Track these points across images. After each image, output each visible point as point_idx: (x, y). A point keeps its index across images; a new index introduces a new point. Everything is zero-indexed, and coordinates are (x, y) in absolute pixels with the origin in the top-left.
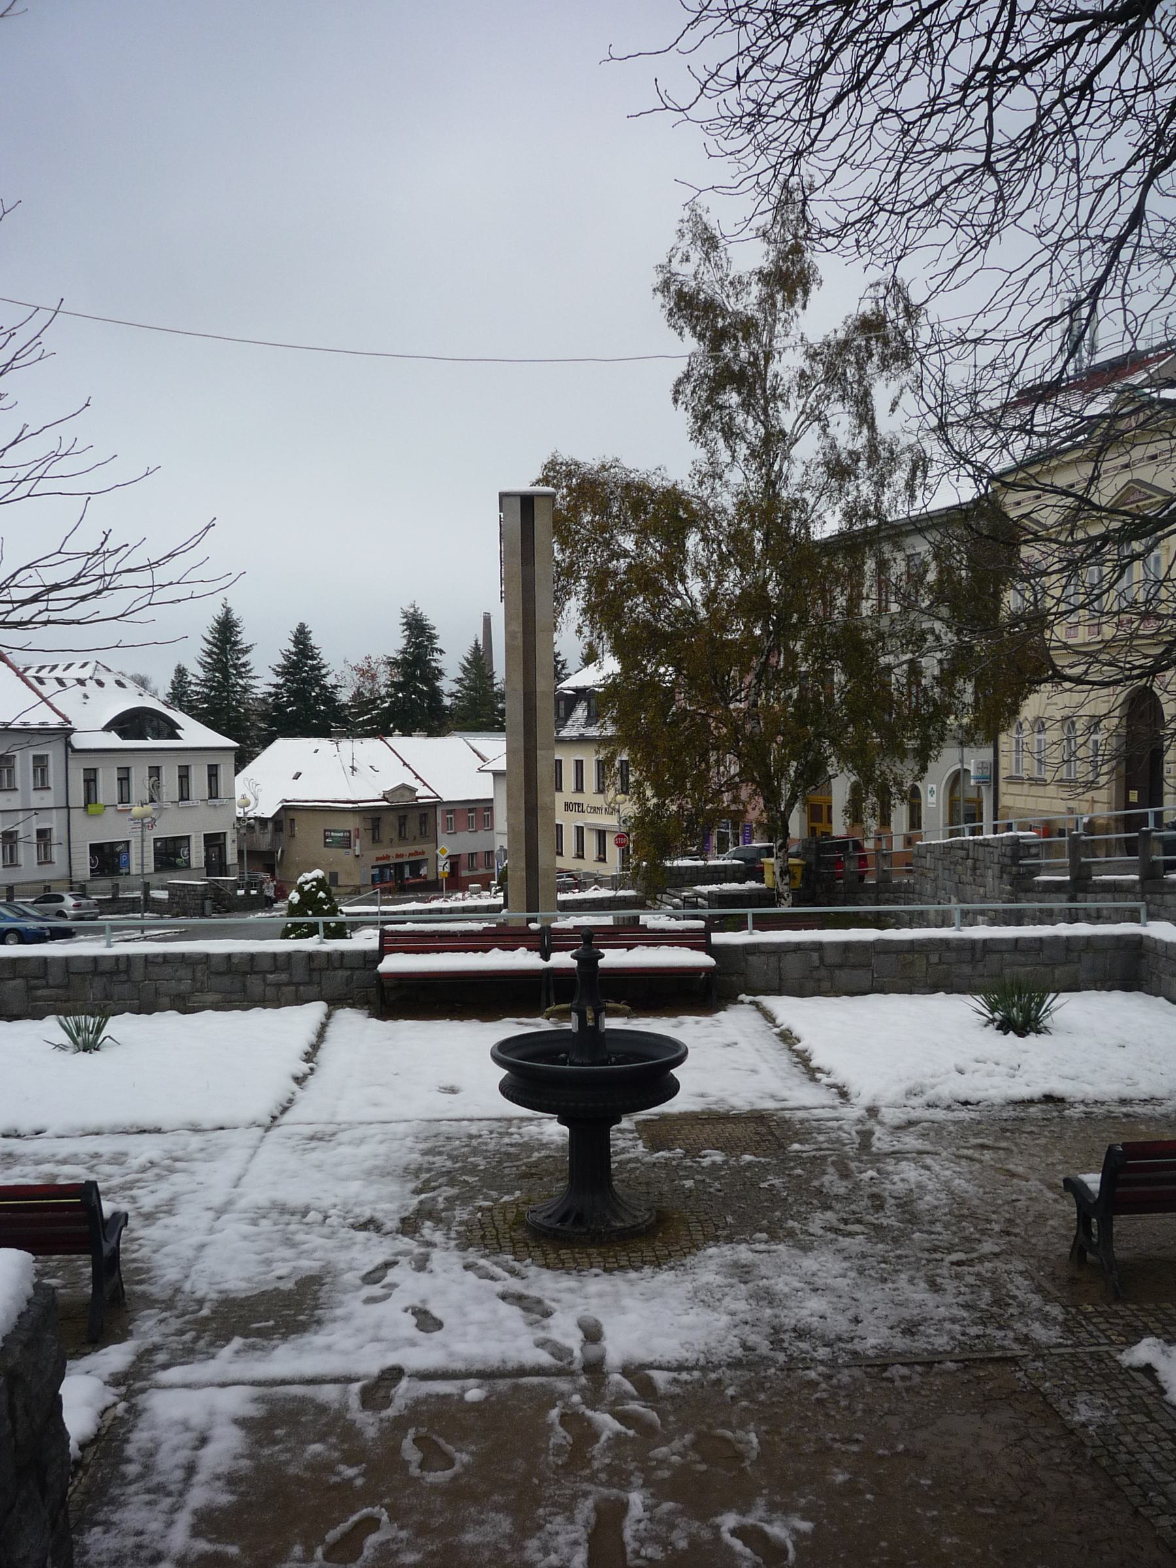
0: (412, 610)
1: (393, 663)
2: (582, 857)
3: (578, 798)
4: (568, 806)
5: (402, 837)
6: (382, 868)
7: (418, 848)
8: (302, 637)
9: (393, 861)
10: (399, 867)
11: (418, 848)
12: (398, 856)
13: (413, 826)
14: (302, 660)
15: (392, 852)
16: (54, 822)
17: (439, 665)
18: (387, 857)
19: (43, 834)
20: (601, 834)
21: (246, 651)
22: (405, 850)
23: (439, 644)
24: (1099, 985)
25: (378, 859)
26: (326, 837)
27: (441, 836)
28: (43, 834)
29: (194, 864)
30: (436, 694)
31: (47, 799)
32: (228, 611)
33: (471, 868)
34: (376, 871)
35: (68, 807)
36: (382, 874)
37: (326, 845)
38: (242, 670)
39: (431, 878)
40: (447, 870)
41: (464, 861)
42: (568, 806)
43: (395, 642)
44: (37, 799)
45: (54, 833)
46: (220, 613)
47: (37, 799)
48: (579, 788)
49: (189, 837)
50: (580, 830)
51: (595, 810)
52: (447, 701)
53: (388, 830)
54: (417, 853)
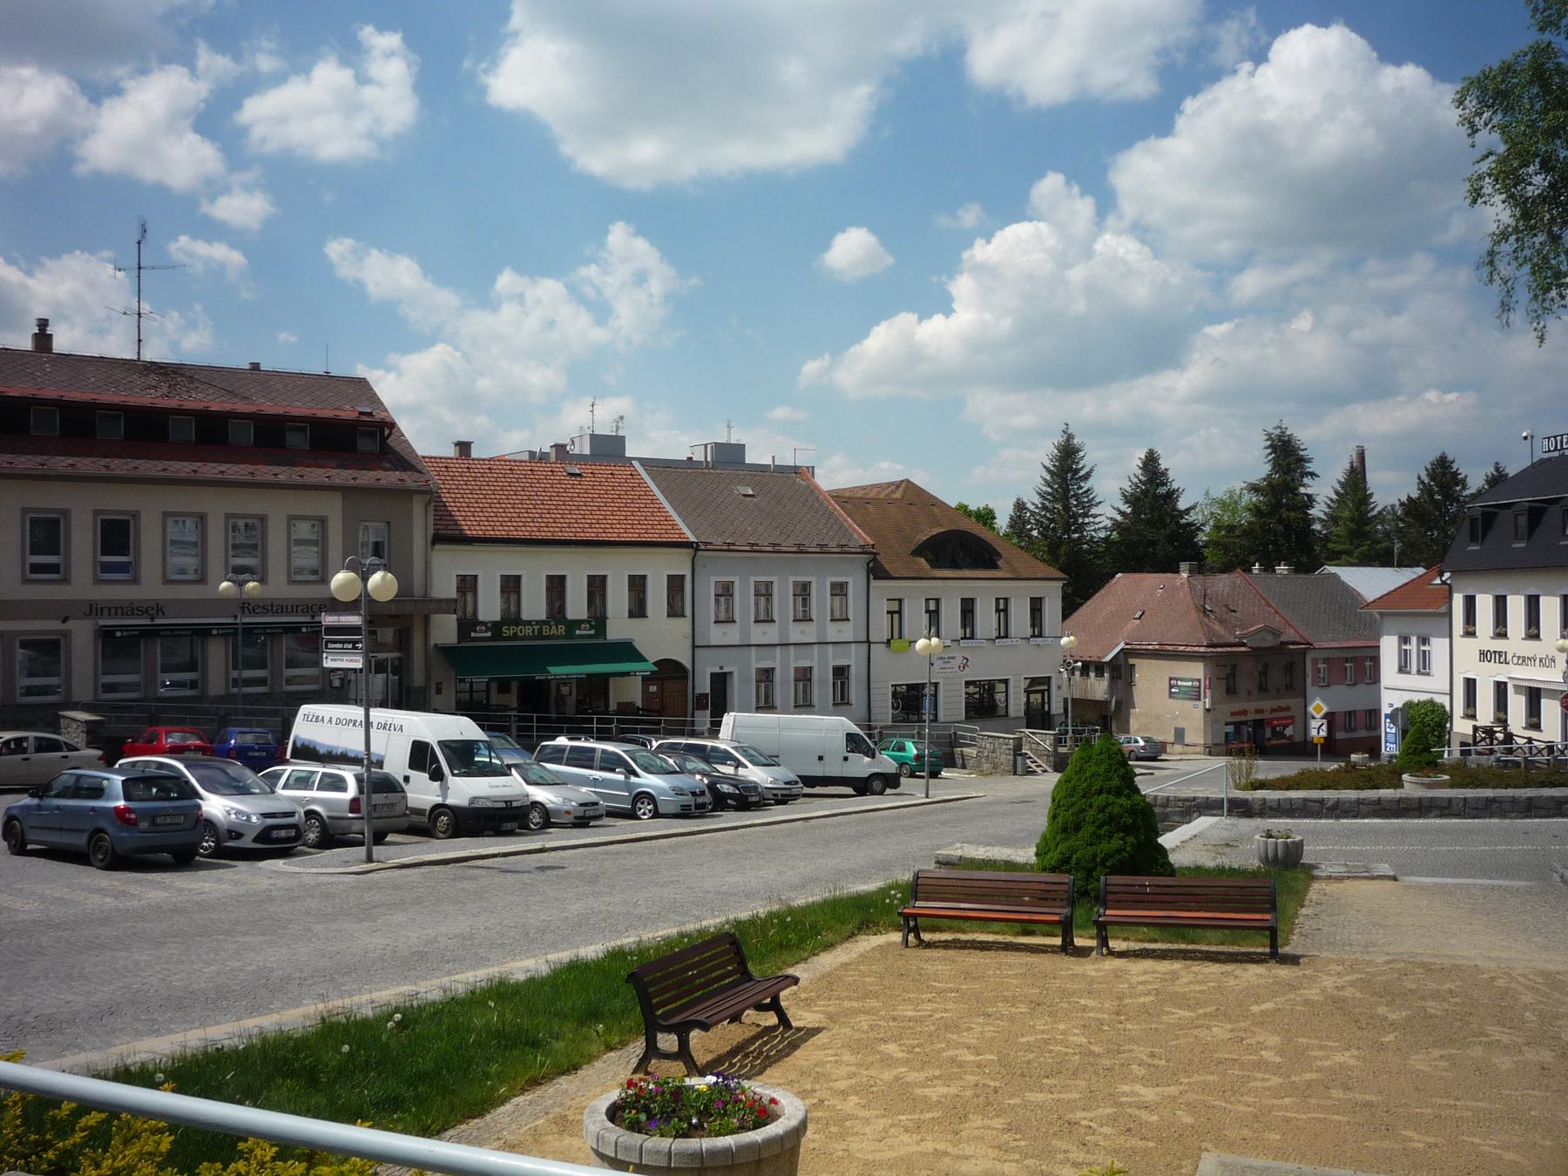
0: (1278, 432)
1: (1254, 488)
2: (1537, 637)
3: (1499, 645)
4: (1484, 655)
5: (1263, 689)
6: (1237, 725)
7: (1282, 703)
8: (1151, 462)
9: (1250, 717)
10: (1258, 724)
11: (1282, 703)
12: (1258, 711)
13: (1276, 678)
14: (1153, 493)
15: (1251, 706)
16: (853, 658)
17: (1309, 491)
18: (1244, 712)
19: (841, 672)
20: (1534, 696)
21: (1087, 477)
22: (1267, 704)
23: (1311, 467)
24: (1079, 600)
25: (1233, 714)
26: (1171, 687)
27: (1310, 689)
28: (841, 672)
29: (1012, 713)
30: (1308, 521)
31: (847, 632)
32: (1070, 437)
33: (1349, 729)
34: (1230, 729)
35: (868, 642)
36: (1238, 732)
37: (1171, 695)
38: (1087, 503)
39: (1298, 738)
40: (1323, 733)
41: (1339, 720)
42: (1484, 655)
43: (1258, 466)
44: (834, 632)
45: (853, 671)
46: (1059, 439)
47: (834, 632)
48: (1501, 631)
49: (1049, 678)
50: (1501, 688)
51: (1524, 660)
52: (1317, 527)
53: (1245, 682)
54: (1281, 709)
